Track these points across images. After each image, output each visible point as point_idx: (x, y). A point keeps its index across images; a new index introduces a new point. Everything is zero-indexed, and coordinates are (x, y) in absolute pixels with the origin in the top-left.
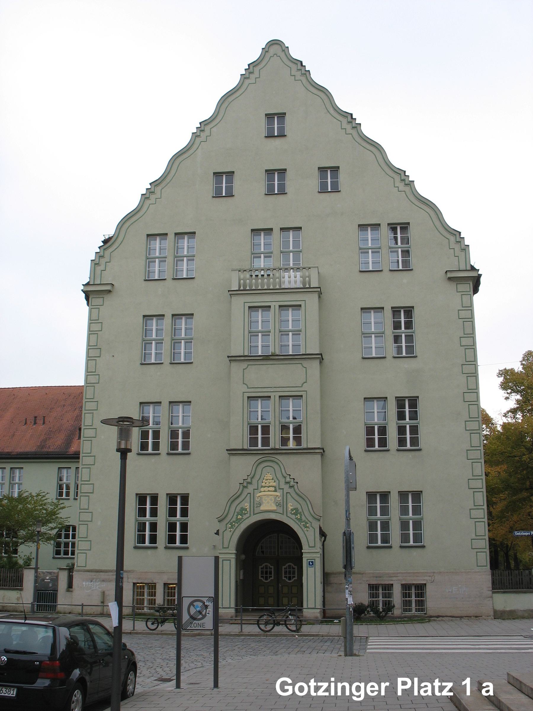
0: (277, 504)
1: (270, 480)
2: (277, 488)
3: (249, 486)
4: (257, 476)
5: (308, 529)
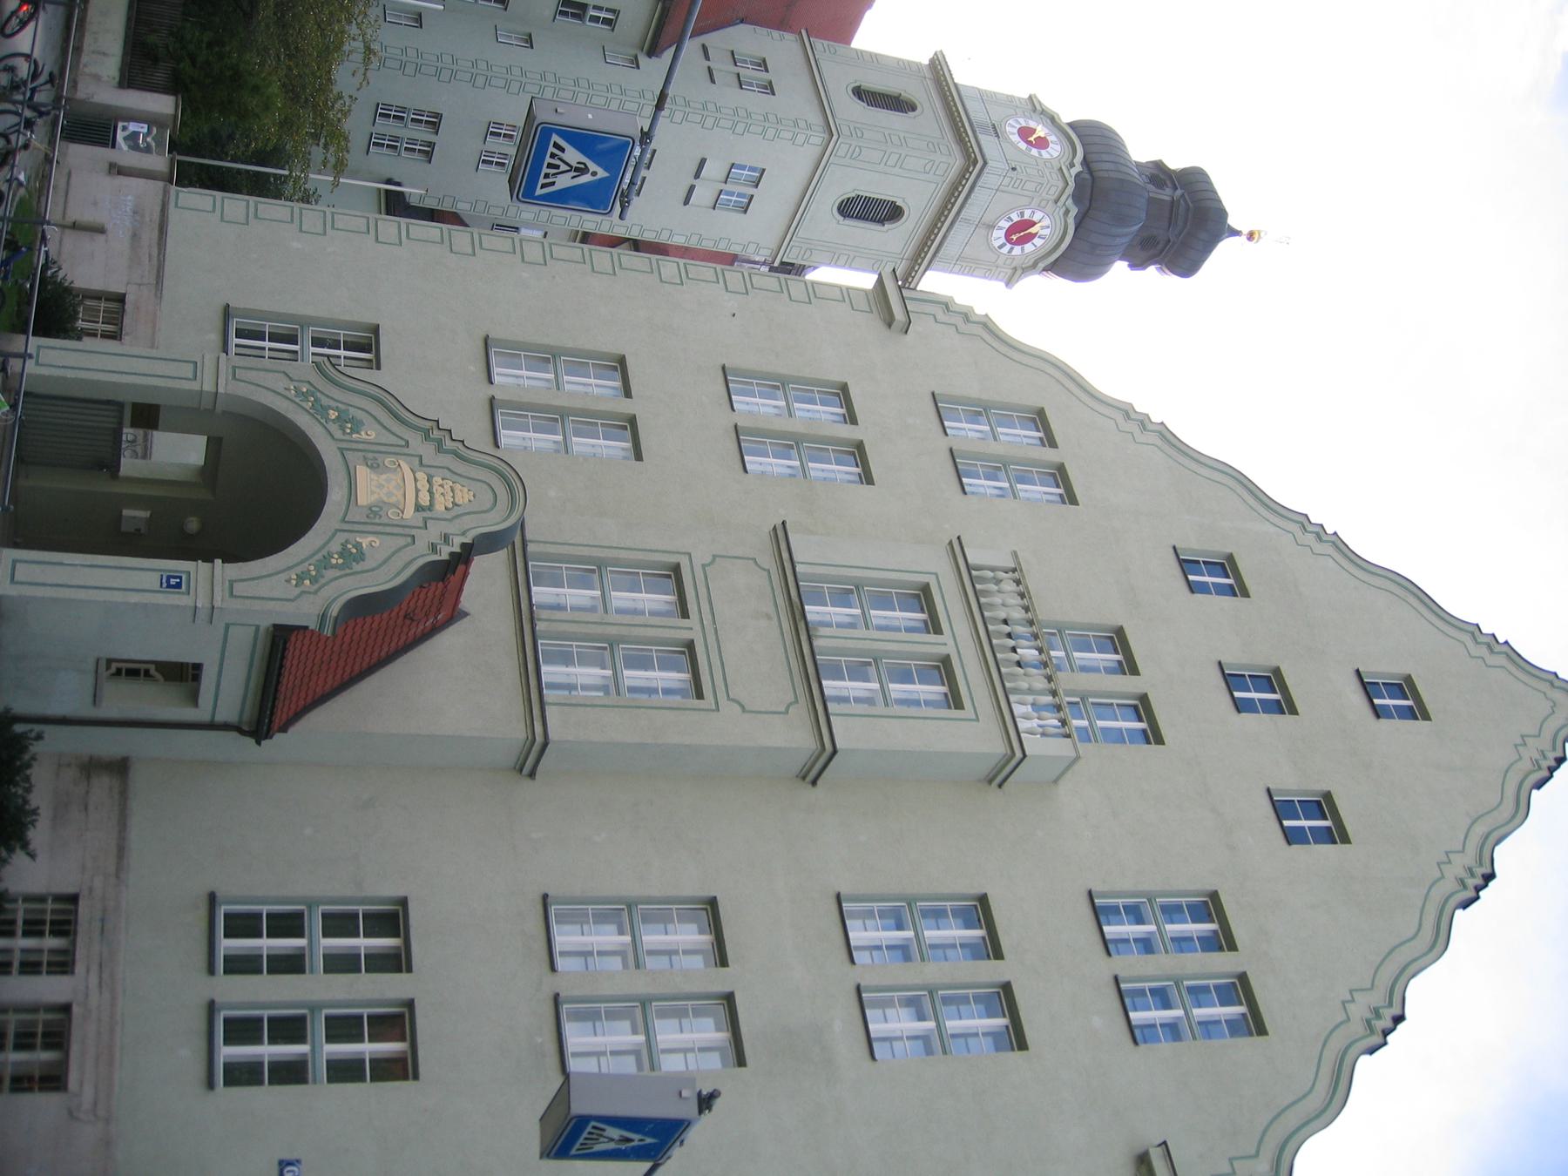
0: (377, 509)
2: (427, 514)
5: (294, 582)
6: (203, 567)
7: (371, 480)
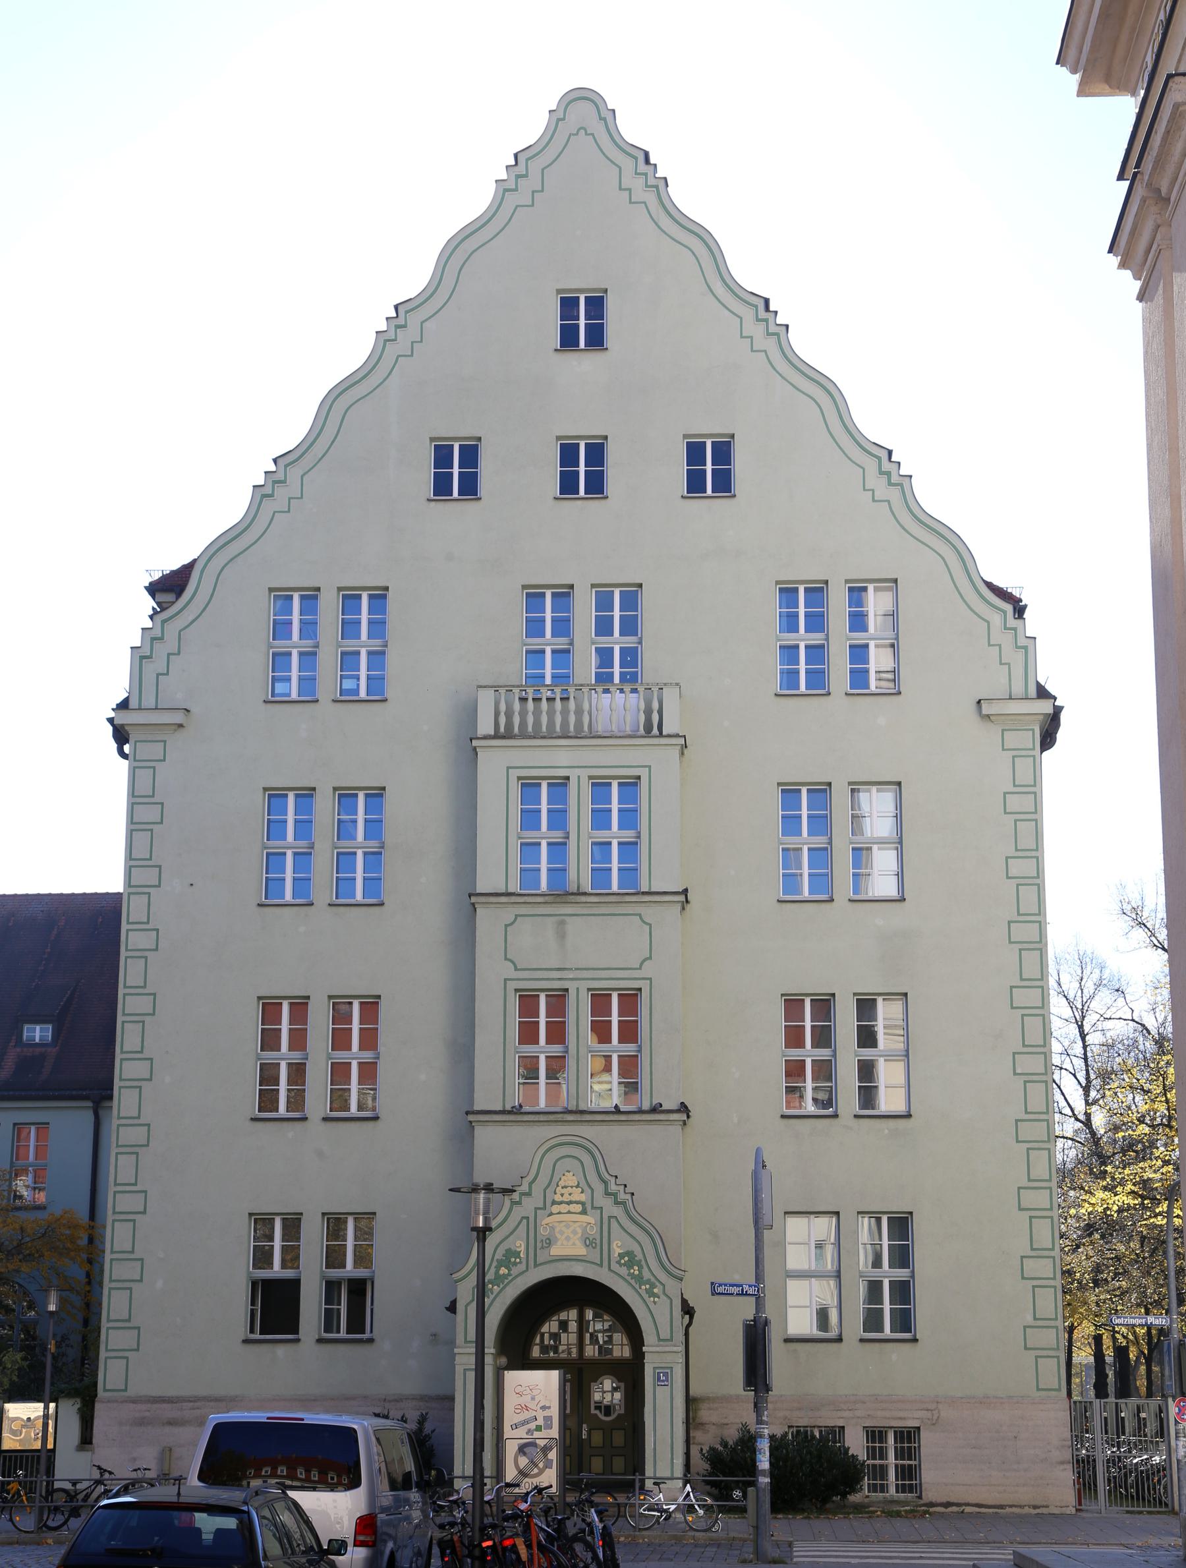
1: (572, 1187)
2: (589, 1206)
3: (525, 1199)
4: (543, 1180)
5: (656, 1299)
6: (458, 1359)
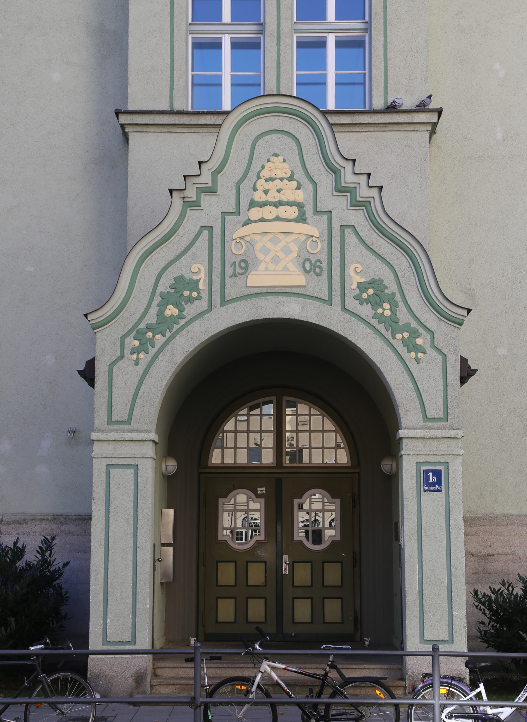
5: (420, 355)
7: (267, 270)
